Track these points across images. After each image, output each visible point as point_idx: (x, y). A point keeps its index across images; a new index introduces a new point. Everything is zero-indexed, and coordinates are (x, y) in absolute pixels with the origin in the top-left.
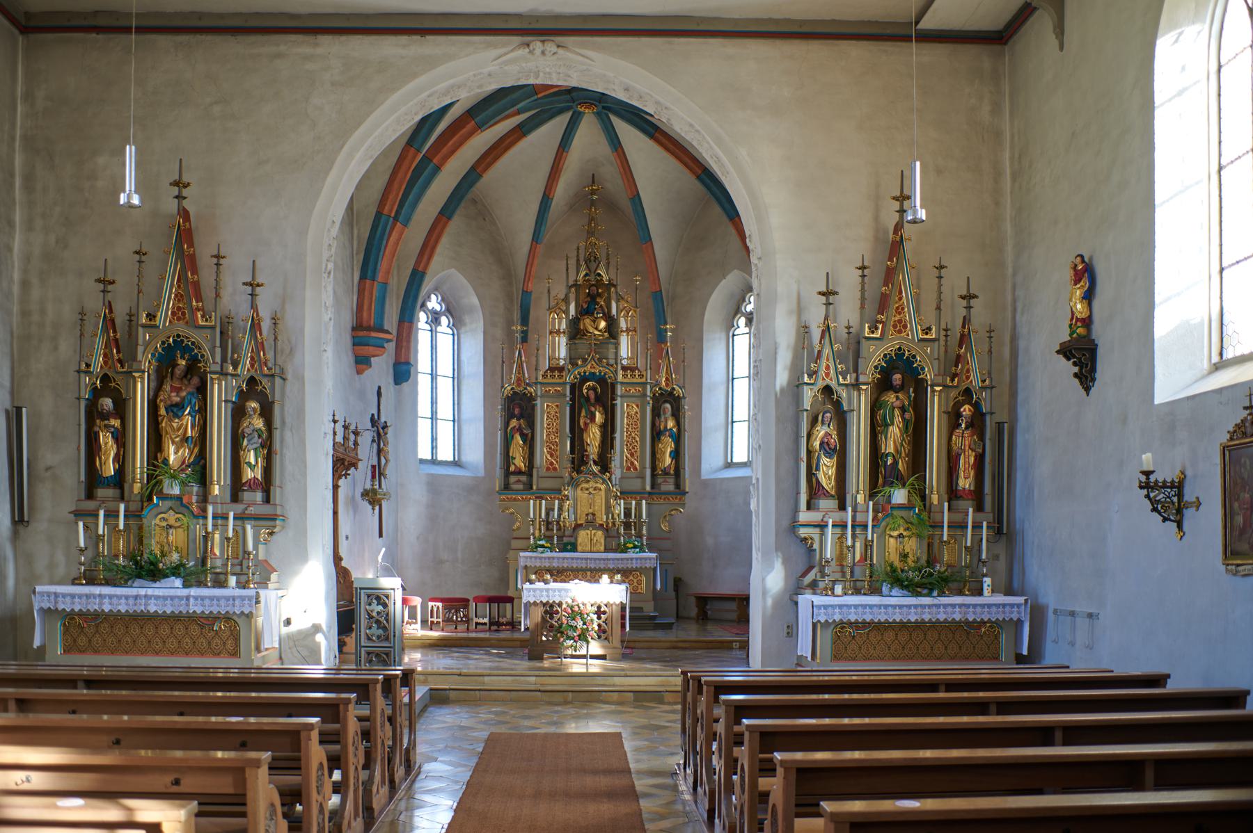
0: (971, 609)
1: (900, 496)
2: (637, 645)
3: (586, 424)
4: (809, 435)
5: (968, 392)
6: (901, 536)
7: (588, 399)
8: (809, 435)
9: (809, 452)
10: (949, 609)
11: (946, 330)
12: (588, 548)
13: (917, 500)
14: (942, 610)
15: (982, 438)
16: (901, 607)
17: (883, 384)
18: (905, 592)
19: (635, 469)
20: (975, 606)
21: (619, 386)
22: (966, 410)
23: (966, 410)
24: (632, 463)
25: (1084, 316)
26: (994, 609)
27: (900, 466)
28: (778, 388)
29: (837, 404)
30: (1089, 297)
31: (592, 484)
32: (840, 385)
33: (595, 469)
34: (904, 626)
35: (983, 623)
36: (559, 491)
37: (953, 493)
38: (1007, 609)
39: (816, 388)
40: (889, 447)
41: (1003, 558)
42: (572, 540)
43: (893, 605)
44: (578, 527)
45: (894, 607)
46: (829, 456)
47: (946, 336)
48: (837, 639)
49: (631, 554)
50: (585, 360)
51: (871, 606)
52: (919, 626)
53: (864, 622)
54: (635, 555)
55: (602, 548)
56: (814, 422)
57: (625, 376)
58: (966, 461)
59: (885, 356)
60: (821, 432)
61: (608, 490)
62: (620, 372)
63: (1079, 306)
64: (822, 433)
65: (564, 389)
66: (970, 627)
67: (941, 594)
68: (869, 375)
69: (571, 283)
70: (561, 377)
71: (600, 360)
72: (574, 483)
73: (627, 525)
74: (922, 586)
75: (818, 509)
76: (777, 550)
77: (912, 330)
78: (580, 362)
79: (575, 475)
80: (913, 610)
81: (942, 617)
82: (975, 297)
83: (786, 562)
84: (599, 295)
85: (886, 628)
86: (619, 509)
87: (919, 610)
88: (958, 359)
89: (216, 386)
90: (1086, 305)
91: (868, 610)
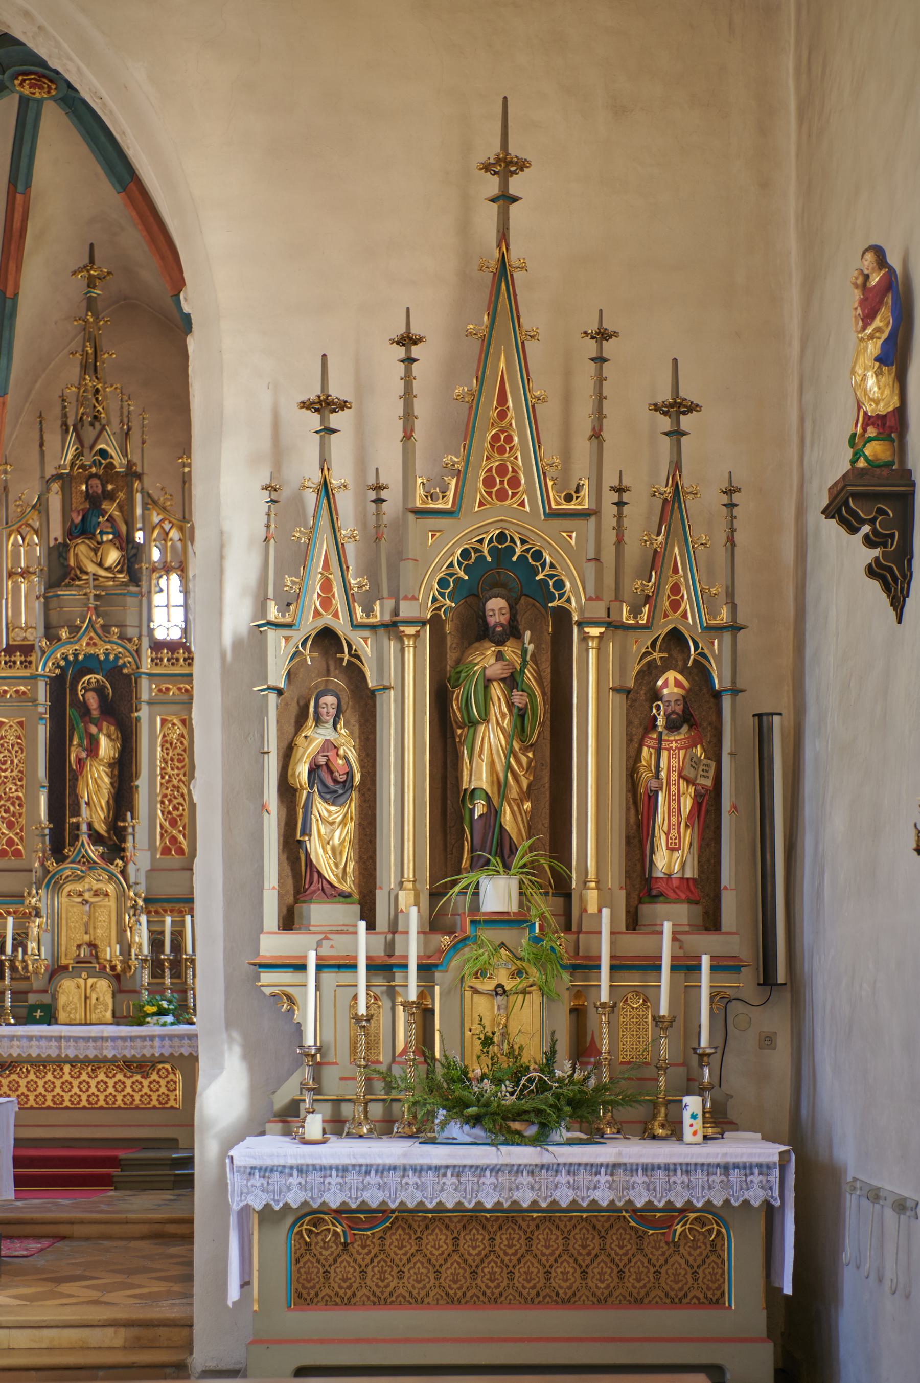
0: (640, 1178)
1: (497, 893)
2: (77, 1230)
3: (80, 761)
4: (288, 754)
5: (676, 638)
6: (500, 991)
7: (84, 710)
8: (288, 754)
9: (287, 791)
10: (583, 1177)
11: (620, 490)
12: (79, 1016)
13: (543, 906)
14: (563, 1178)
15: (715, 754)
16: (458, 1170)
17: (464, 628)
18: (478, 1132)
19: (181, 851)
20: (649, 1169)
21: (144, 682)
22: (671, 684)
23: (671, 684)
24: (174, 840)
25: (882, 409)
26: (699, 1178)
27: (507, 818)
28: (227, 640)
29: (354, 673)
30: (895, 356)
31: (91, 882)
32: (356, 626)
33: (93, 852)
34: (472, 1218)
35: (673, 1213)
36: (19, 897)
37: (642, 888)
38: (735, 1177)
39: (298, 636)
40: (478, 775)
41: (783, 1042)
42: (46, 999)
43: (458, 1167)
44: (57, 971)
45: (441, 1170)
46: (333, 796)
47: (620, 504)
48: (302, 1253)
49: (152, 1028)
50: (74, 630)
51: (382, 1170)
52: (510, 1217)
53: (363, 1208)
54: (157, 1030)
55: (109, 1015)
56: (300, 717)
57: (156, 661)
58: (674, 807)
59: (465, 554)
60: (315, 738)
61: (121, 896)
62: (147, 655)
63: (871, 381)
64: (317, 742)
65: (35, 689)
66: (643, 1220)
67: (595, 1136)
68: (423, 596)
69: (50, 471)
70: (27, 664)
71: (106, 628)
72: (52, 882)
73: (157, 968)
74: (519, 1115)
75: (306, 928)
76: (229, 1025)
77: (530, 491)
78: (64, 634)
79: (51, 864)
80: (488, 1179)
81: (564, 1198)
82: (692, 408)
83: (250, 1055)
84: (111, 496)
85: (428, 1224)
86: (141, 937)
87: (505, 1178)
88: (656, 561)
89: (592, 654)
90: (888, 377)
91: (373, 1179)
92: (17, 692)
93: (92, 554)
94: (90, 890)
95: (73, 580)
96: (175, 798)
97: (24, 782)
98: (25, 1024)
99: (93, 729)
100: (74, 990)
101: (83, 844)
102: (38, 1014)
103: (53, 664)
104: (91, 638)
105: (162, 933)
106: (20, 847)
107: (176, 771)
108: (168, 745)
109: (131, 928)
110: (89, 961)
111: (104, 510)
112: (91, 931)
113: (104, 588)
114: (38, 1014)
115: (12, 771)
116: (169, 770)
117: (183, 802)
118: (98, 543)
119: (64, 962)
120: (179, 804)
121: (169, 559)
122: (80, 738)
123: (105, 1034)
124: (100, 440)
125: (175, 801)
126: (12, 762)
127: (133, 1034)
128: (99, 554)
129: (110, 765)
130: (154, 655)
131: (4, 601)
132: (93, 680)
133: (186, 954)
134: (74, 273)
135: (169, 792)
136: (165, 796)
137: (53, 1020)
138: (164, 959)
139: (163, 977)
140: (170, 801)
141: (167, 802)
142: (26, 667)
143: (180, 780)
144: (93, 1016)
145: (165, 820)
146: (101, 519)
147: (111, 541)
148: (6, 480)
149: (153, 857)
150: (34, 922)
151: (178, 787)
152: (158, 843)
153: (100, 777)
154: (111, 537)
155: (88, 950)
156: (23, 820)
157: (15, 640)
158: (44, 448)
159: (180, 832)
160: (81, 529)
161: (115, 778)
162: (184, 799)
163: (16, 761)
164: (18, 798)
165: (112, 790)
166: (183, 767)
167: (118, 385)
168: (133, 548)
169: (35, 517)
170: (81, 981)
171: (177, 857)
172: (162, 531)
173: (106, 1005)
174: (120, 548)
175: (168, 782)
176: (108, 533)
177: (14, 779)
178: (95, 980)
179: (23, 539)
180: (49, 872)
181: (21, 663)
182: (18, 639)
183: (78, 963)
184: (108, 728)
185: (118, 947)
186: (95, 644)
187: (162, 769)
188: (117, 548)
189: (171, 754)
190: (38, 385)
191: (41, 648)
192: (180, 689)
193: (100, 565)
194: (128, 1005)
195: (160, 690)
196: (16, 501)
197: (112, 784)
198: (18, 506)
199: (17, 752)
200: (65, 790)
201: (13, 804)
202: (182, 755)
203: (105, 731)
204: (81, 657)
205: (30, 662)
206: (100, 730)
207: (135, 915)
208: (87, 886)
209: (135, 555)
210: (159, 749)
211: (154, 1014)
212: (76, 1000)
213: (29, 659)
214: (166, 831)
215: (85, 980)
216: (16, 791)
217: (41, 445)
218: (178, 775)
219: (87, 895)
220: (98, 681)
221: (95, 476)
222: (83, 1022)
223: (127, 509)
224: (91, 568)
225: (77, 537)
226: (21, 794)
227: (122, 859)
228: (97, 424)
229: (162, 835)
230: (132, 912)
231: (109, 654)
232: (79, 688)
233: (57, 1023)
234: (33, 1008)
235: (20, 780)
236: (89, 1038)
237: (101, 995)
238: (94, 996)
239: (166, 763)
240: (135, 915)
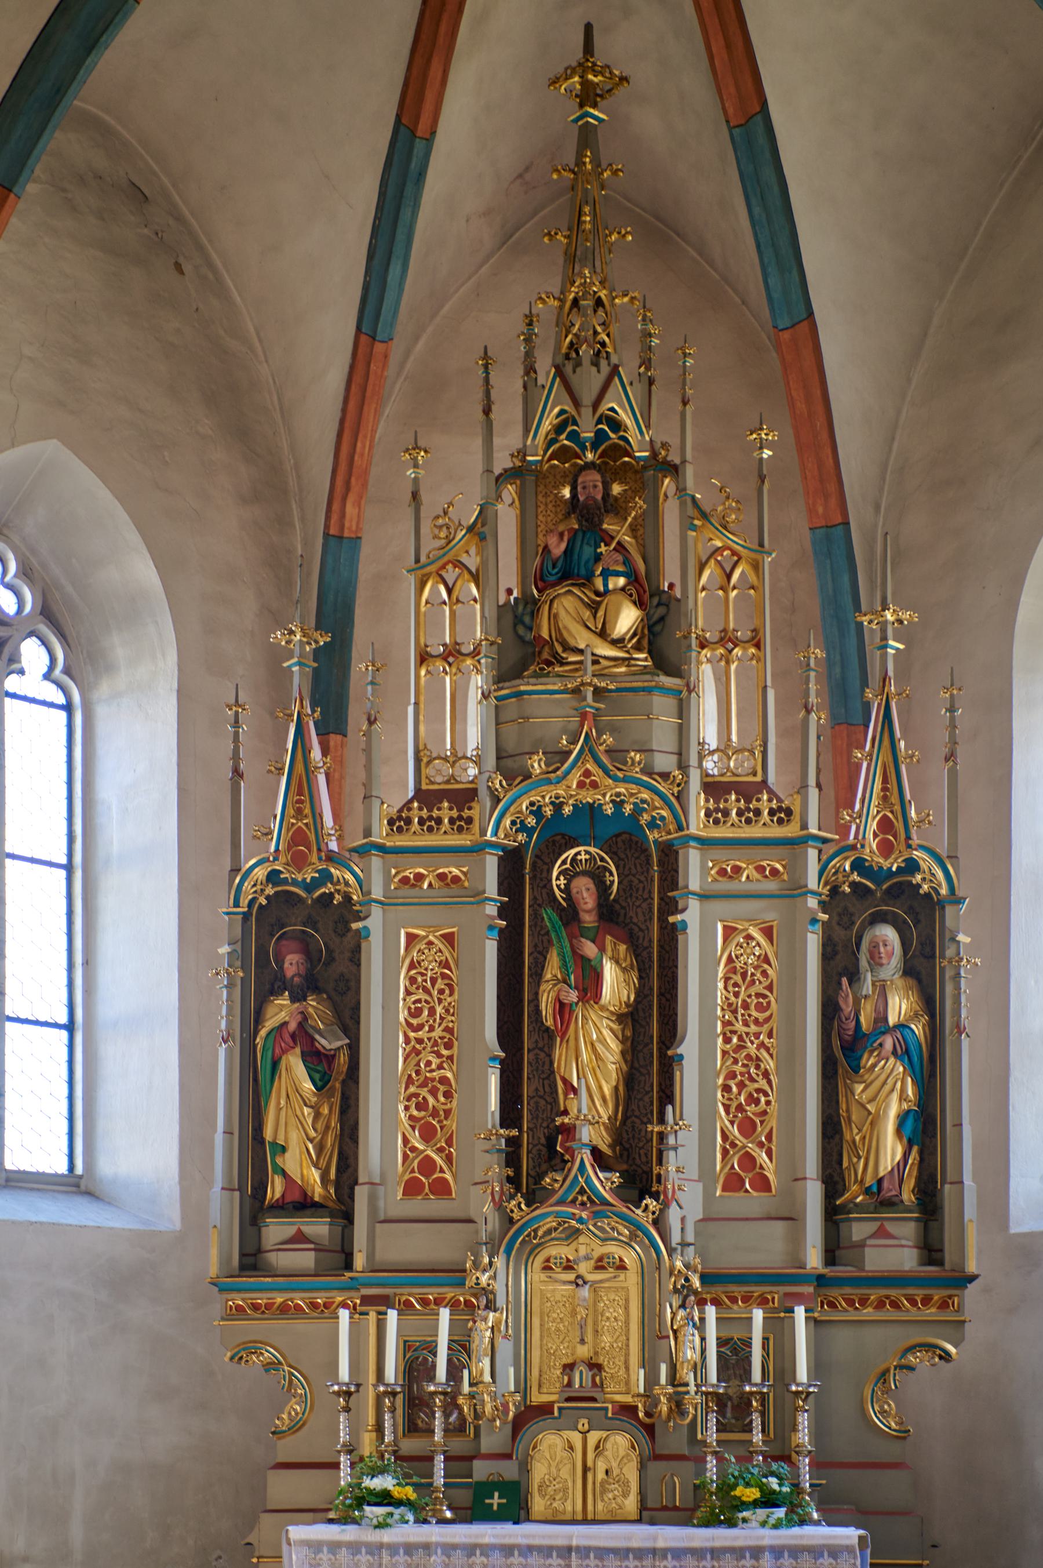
3: (563, 1009)
12: (573, 1505)
19: (763, 1184)
24: (748, 1161)
31: (587, 1246)
33: (603, 1183)
36: (456, 1274)
42: (509, 1470)
44: (530, 1416)
54: (768, 1537)
61: (652, 1271)
62: (698, 803)
72: (515, 1240)
73: (733, 1410)
78: (537, 765)
79: (516, 1205)
92: (442, 877)
93: (587, 614)
94: (587, 1258)
95: (549, 663)
96: (752, 1080)
97: (455, 1050)
98: (471, 1522)
99: (590, 949)
100: (560, 1453)
101: (582, 1167)
102: (496, 1501)
103: (513, 823)
104: (587, 773)
105: (748, 1343)
106: (448, 1176)
107: (753, 1028)
108: (738, 978)
109: (675, 1332)
110: (583, 1398)
111: (605, 531)
112: (589, 1337)
113: (613, 677)
114: (496, 1501)
115: (432, 1029)
116: (739, 1026)
117: (767, 1088)
118: (597, 593)
119: (537, 1398)
120: (759, 1091)
121: (732, 626)
122: (564, 965)
123: (661, 1544)
124: (608, 396)
125: (752, 1087)
126: (432, 1012)
127: (717, 1544)
128: (601, 613)
129: (620, 1018)
130: (711, 805)
131: (411, 709)
132: (583, 857)
133: (798, 1385)
134: (555, 82)
135: (738, 1068)
136: (732, 1075)
137: (523, 1513)
138: (752, 1393)
139: (748, 1429)
140: (741, 1086)
141: (735, 1089)
142: (460, 829)
143: (762, 1045)
144: (600, 1506)
145: (732, 1123)
146: (603, 549)
147: (623, 589)
148: (416, 479)
149: (708, 1197)
150: (485, 1319)
151: (758, 1059)
152: (718, 1168)
153: (603, 1041)
154: (622, 581)
155: (587, 1375)
156: (452, 1124)
157: (432, 783)
158: (492, 416)
159: (761, 1145)
160: (564, 571)
161: (629, 1044)
162: (769, 1082)
163: (439, 1010)
164: (444, 1080)
165: (625, 1067)
166: (768, 1020)
167: (636, 294)
168: (659, 604)
169: (473, 550)
170: (576, 1438)
171: (755, 1194)
172: (719, 571)
173: (626, 1484)
174: (640, 604)
175: (740, 1048)
176: (618, 574)
177: (436, 1044)
178: (604, 1434)
179: (450, 591)
180: (511, 1221)
181: (452, 821)
182: (439, 779)
183: (569, 1399)
184: (615, 949)
185: (642, 1372)
186: (594, 785)
187: (726, 1024)
188: (635, 603)
189: (742, 996)
190: (420, 345)
191: (491, 791)
192: (761, 869)
193: (603, 634)
194: (678, 1483)
195: (722, 872)
196: (437, 517)
197: (623, 1053)
198: (440, 527)
199: (441, 992)
200: (521, 1069)
201: (434, 1092)
202: (765, 996)
203: (609, 953)
204: (567, 810)
205: (469, 821)
206: (602, 949)
207: (683, 1306)
208: (583, 1251)
209: (662, 619)
210: (721, 985)
211: (756, 1504)
212: (565, 1473)
213: (466, 813)
214: (733, 1145)
215: (584, 1433)
216: (440, 1067)
217: (487, 411)
218: (757, 1035)
219: (584, 1268)
220: (592, 858)
221: (590, 466)
222: (580, 1517)
223: (647, 531)
224: (582, 638)
225: (554, 585)
226: (449, 1075)
227: (655, 1196)
228: (603, 363)
229: (725, 1152)
230: (676, 1301)
231: (622, 802)
232: (555, 874)
233: (528, 1520)
234: (484, 1489)
235: (448, 1046)
236: (628, 1550)
237: (614, 1465)
238: (601, 1466)
239: (735, 1012)
240: (683, 1306)
